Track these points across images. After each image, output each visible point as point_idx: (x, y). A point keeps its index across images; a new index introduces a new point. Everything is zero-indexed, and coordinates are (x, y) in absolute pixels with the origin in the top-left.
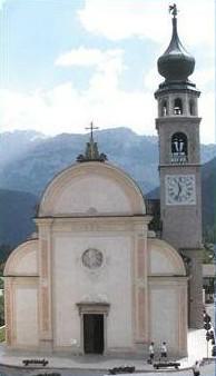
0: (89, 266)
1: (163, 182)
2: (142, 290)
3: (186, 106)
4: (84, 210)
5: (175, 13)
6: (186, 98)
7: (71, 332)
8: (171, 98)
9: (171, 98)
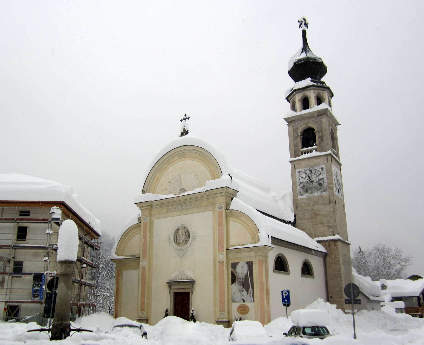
3: (313, 101)
6: (326, 95)
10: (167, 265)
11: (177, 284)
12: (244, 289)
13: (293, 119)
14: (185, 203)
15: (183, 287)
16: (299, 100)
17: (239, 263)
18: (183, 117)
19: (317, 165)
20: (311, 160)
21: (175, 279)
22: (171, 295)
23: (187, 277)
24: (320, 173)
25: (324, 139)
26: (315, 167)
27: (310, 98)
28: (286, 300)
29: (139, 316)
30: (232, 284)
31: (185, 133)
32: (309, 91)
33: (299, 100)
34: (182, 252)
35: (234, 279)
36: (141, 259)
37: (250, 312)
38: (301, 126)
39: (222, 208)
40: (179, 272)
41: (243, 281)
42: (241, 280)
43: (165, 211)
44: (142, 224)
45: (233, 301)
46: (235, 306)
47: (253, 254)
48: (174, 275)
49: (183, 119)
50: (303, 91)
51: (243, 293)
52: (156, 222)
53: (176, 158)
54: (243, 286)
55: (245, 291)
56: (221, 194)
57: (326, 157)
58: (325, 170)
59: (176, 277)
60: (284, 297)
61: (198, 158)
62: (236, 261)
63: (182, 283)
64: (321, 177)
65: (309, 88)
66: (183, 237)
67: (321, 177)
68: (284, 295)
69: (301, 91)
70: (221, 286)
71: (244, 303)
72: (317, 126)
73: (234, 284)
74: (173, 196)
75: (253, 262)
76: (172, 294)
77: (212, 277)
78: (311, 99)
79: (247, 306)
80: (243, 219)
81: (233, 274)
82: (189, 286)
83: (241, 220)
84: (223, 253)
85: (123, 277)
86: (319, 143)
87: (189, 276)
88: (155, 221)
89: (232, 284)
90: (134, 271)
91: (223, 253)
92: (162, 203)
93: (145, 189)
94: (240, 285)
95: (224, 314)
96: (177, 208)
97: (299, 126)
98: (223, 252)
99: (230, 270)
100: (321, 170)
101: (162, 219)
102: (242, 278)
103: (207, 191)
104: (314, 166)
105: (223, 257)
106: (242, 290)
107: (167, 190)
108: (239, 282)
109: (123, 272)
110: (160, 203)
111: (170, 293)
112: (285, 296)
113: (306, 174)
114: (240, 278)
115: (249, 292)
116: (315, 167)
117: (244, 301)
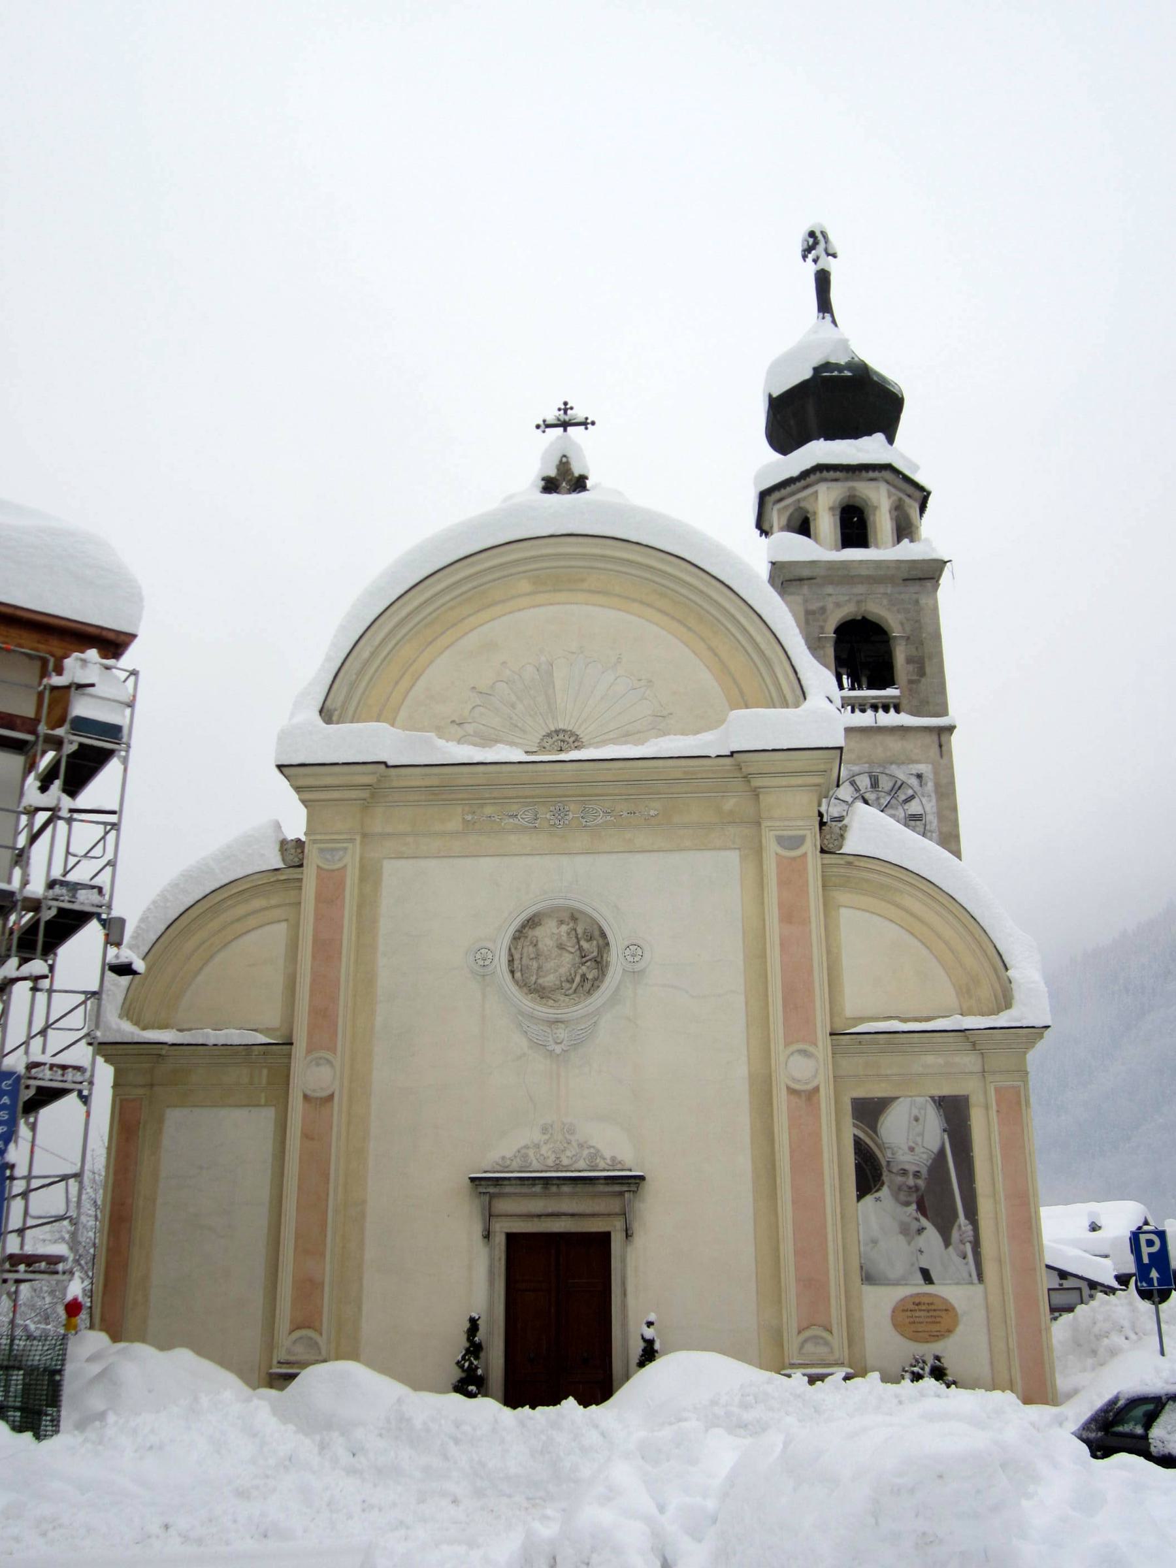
0: (539, 992)
3: (883, 523)
10: (460, 1095)
11: (538, 1189)
12: (924, 1222)
13: (806, 573)
14: (565, 796)
15: (566, 1206)
16: (832, 509)
17: (892, 1100)
18: (552, 415)
19: (900, 763)
20: (879, 738)
21: (515, 1165)
22: (492, 1249)
24: (910, 792)
25: (928, 670)
26: (894, 770)
27: (876, 508)
28: (1154, 1274)
29: (283, 1356)
30: (860, 1197)
31: (564, 480)
32: (873, 484)
33: (832, 509)
34: (562, 1033)
35: (869, 1173)
37: (960, 1329)
38: (838, 605)
39: (799, 841)
40: (544, 1130)
41: (921, 1183)
42: (911, 1181)
43: (455, 824)
44: (310, 876)
45: (869, 1278)
46: (879, 1303)
47: (969, 1061)
48: (511, 1147)
49: (551, 419)
50: (846, 479)
51: (921, 1241)
52: (394, 873)
53: (524, 586)
54: (922, 1208)
55: (932, 1234)
56: (799, 781)
57: (935, 738)
58: (930, 786)
59: (522, 1153)
60: (1146, 1260)
61: (649, 605)
62: (877, 1090)
63: (566, 1189)
65: (871, 474)
66: (566, 961)
68: (1145, 1251)
69: (838, 474)
70: (808, 1205)
71: (929, 1289)
72: (900, 617)
73: (869, 1199)
74: (517, 755)
75: (973, 1100)
76: (500, 1240)
77: (744, 1162)
78: (877, 513)
79: (945, 1301)
80: (908, 902)
81: (861, 1150)
83: (898, 906)
84: (811, 1049)
85: (166, 1141)
86: (911, 682)
87: (608, 1154)
88: (389, 867)
89: (860, 1197)
90: (239, 1114)
91: (811, 1049)
92: (444, 786)
93: (335, 702)
94: (907, 1204)
95: (827, 1343)
96: (530, 815)
97: (830, 606)
98: (815, 1044)
99: (850, 1131)
100: (914, 781)
101: (433, 863)
102: (912, 1169)
103: (733, 753)
104: (891, 763)
105: (808, 1066)
106: (915, 1226)
107: (470, 728)
108: (897, 1191)
109: (161, 1120)
110: (435, 781)
112: (1150, 1255)
113: (857, 790)
114: (904, 1172)
115: (955, 1235)
116: (894, 770)
117: (927, 1276)
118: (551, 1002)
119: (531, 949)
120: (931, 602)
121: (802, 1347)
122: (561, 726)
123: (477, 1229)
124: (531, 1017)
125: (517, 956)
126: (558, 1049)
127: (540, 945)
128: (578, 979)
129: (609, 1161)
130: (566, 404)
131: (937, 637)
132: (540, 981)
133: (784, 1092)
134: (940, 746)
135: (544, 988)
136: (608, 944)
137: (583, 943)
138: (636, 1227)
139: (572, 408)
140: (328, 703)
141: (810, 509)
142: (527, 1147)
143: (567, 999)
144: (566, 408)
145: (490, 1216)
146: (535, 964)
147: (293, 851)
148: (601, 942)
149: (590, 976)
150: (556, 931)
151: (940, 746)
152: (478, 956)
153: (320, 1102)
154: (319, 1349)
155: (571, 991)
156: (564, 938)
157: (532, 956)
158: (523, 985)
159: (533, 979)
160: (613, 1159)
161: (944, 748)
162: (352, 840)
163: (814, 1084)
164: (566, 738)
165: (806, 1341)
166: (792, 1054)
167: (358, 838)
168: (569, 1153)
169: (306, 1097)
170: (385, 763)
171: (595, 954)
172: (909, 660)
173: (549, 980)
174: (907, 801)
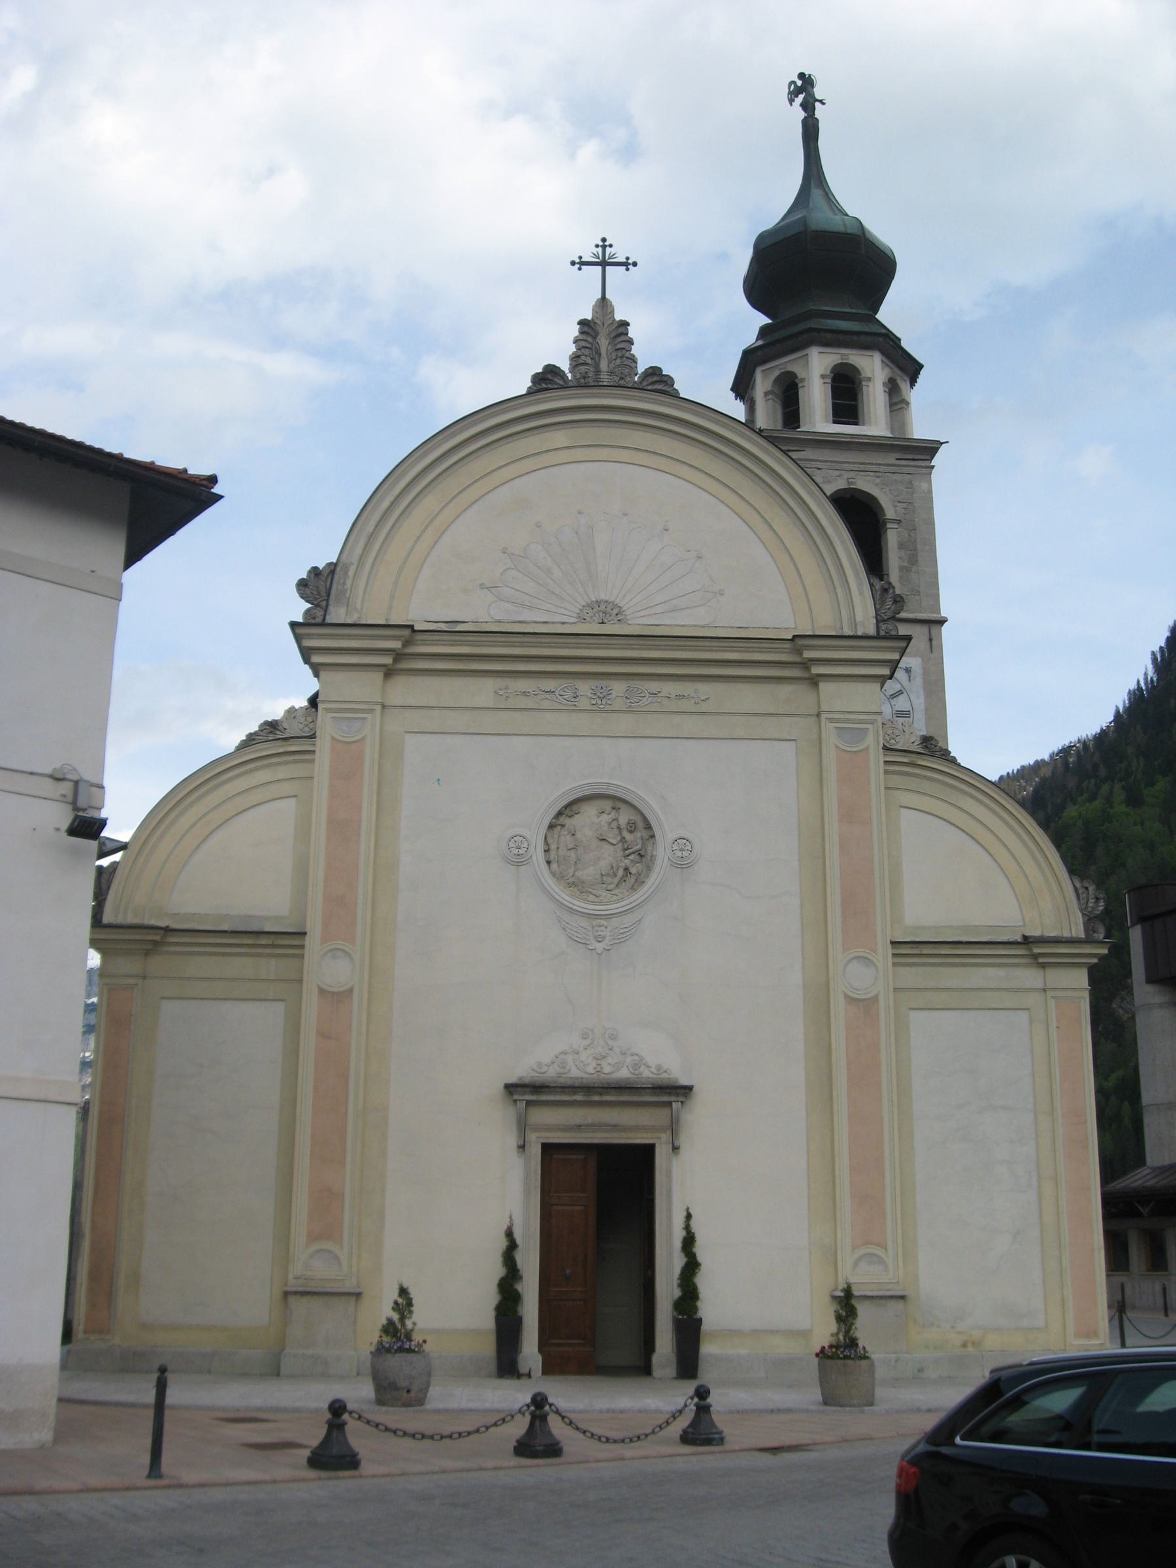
0: (577, 886)
1: (644, 845)
2: (865, 1006)
3: (875, 397)
4: (558, 612)
5: (808, 106)
6: (873, 368)
7: (455, 1223)
8: (816, 367)
9: (816, 367)
23: (636, 1066)
33: (823, 377)
36: (313, 943)
40: (584, 1036)
64: (901, 703)
67: (901, 703)
76: (536, 1151)
82: (657, 1117)
95: (882, 1261)
96: (568, 695)
103: (795, 637)
104: (87, 827)
111: (522, 1147)
118: (591, 898)
119: (569, 838)
120: (924, 486)
121: (856, 1264)
122: (603, 597)
123: (512, 1141)
124: (571, 911)
125: (553, 847)
126: (600, 947)
127: (578, 835)
128: (621, 873)
129: (653, 1070)
130: (604, 240)
131: (930, 523)
132: (579, 874)
133: (316, 991)
134: (931, 640)
135: (583, 882)
136: (653, 836)
137: (625, 834)
138: (683, 1141)
139: (611, 246)
140: (344, 557)
141: (801, 374)
142: (564, 1053)
143: (608, 894)
144: (604, 244)
145: (523, 1127)
146: (572, 854)
147: (302, 720)
148: (645, 834)
149: (633, 870)
150: (596, 820)
151: (931, 640)
152: (512, 845)
153: (336, 998)
154: (340, 1264)
155: (611, 887)
156: (605, 828)
157: (570, 846)
158: (559, 877)
159: (571, 871)
160: (659, 1068)
161: (934, 643)
162: (371, 711)
163: (350, 985)
164: (609, 609)
165: (859, 1259)
166: (850, 961)
167: (378, 708)
168: (610, 1060)
169: (322, 991)
170: (412, 627)
171: (639, 847)
172: (901, 546)
173: (588, 873)
174: (893, 696)
